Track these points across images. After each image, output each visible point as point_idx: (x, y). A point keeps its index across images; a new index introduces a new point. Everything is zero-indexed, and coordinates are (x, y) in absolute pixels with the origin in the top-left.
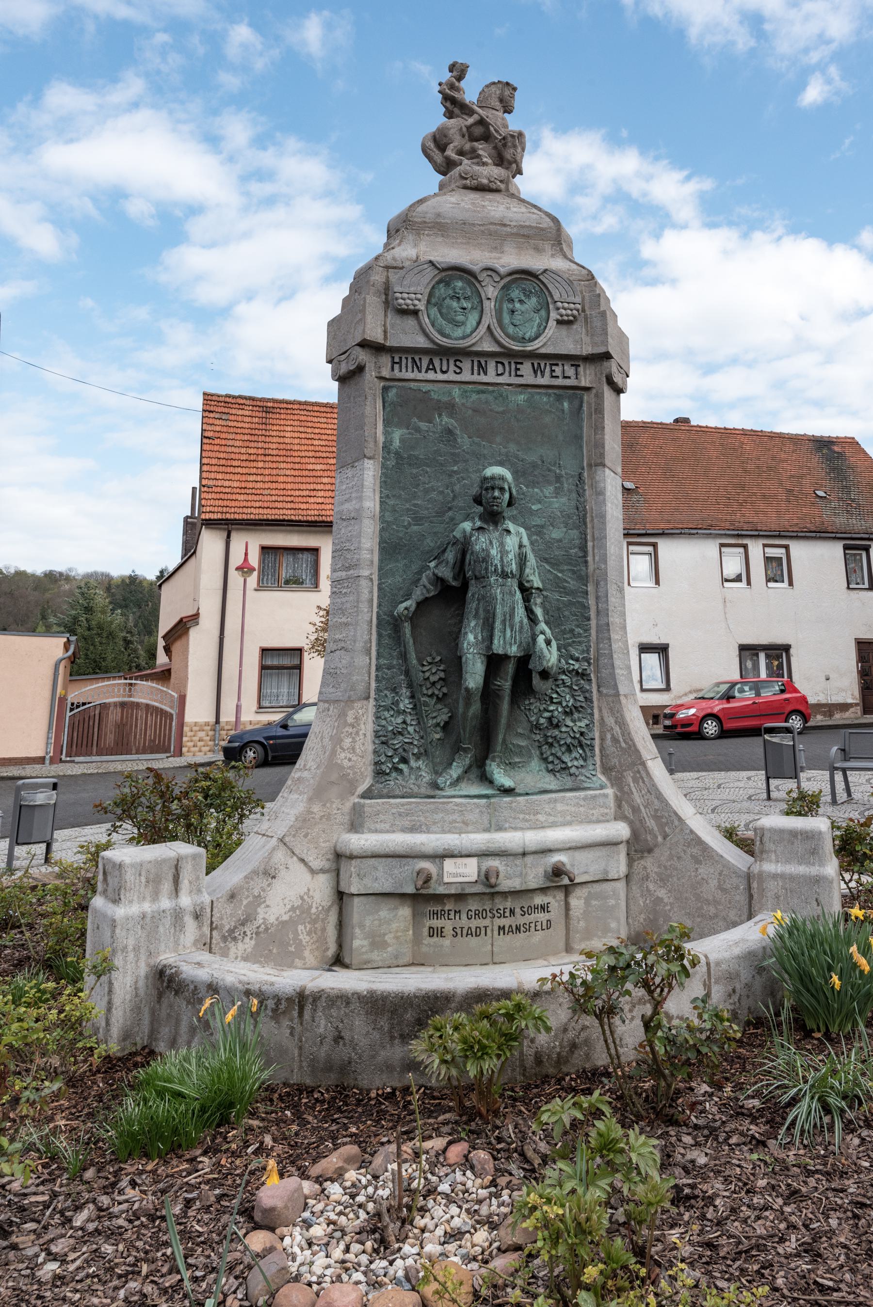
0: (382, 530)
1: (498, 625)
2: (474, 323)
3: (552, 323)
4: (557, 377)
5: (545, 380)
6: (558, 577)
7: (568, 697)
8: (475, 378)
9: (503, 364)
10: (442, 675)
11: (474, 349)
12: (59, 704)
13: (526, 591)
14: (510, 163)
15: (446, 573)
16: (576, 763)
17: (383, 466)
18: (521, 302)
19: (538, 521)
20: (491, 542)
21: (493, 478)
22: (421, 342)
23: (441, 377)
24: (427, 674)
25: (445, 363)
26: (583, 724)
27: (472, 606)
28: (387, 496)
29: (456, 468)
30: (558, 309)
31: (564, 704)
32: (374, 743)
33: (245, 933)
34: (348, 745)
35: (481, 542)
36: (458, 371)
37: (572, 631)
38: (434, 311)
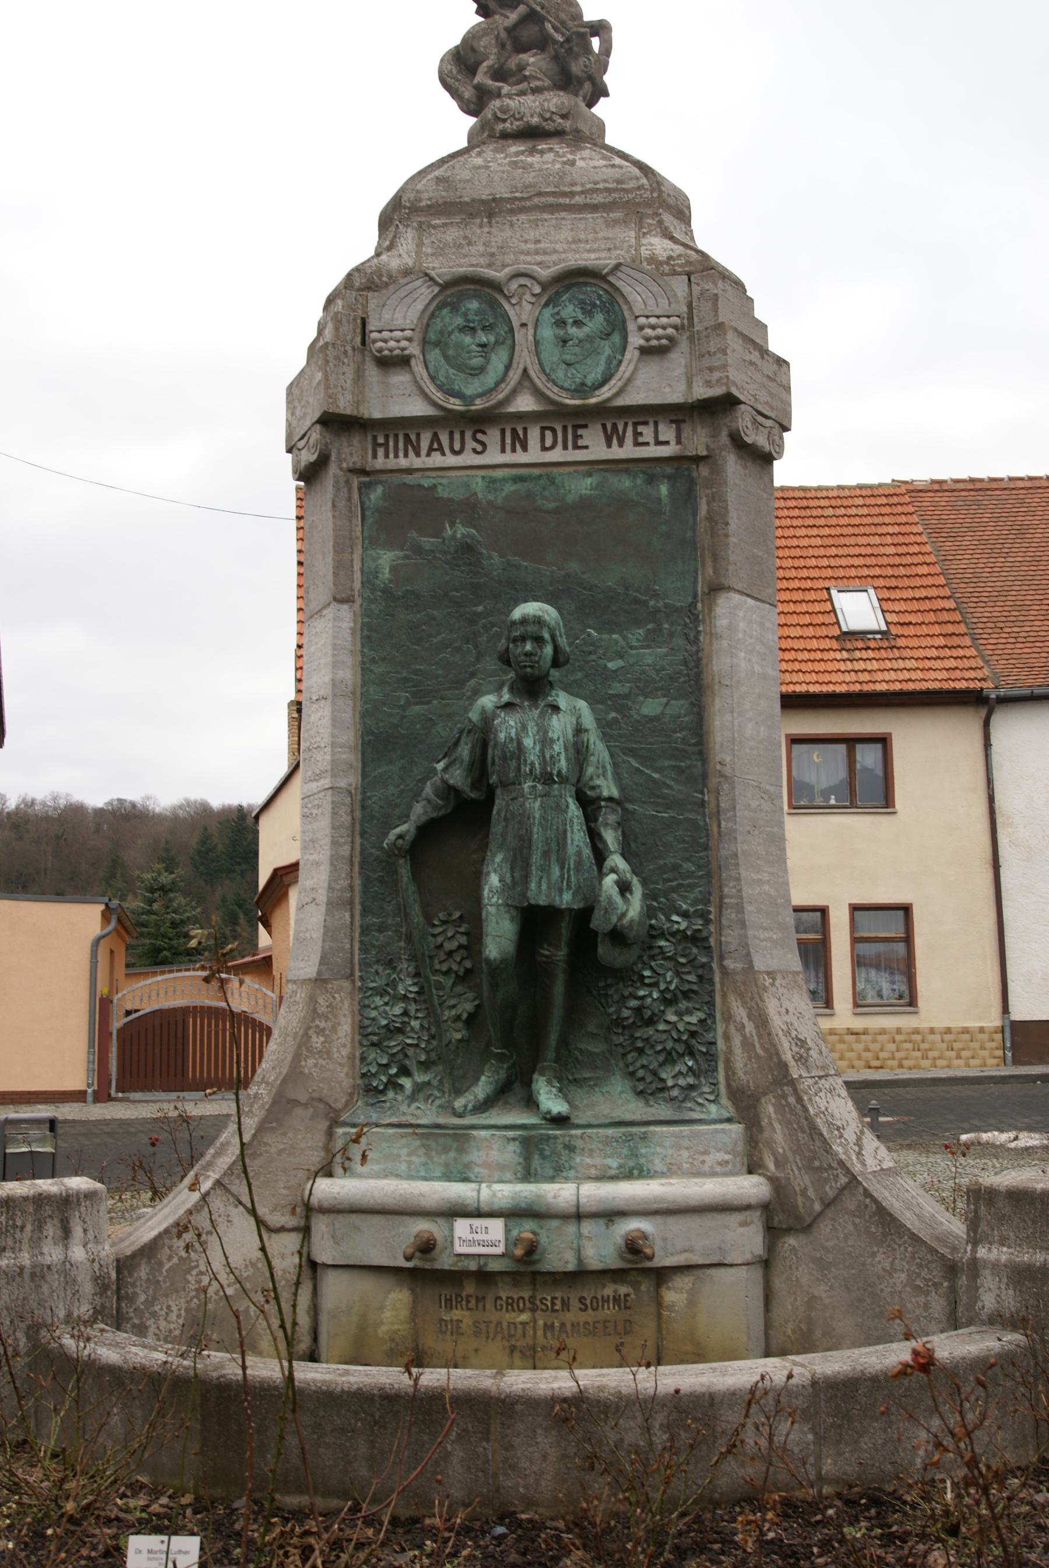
0: (364, 715)
1: (536, 858)
2: (501, 368)
3: (631, 354)
4: (647, 444)
5: (628, 451)
6: (654, 780)
7: (669, 975)
8: (508, 458)
9: (554, 431)
10: (463, 940)
12: (102, 1008)
13: (589, 804)
14: (580, 83)
15: (457, 777)
16: (682, 1082)
18: (577, 323)
19: (617, 688)
20: (524, 727)
21: (524, 621)
22: (417, 408)
23: (451, 460)
24: (440, 939)
25: (457, 437)
26: (694, 1019)
27: (497, 828)
28: (373, 661)
29: (480, 609)
30: (641, 328)
31: (662, 986)
32: (361, 1045)
33: (169, 1307)
35: (507, 726)
36: (479, 448)
37: (676, 867)
38: (434, 355)
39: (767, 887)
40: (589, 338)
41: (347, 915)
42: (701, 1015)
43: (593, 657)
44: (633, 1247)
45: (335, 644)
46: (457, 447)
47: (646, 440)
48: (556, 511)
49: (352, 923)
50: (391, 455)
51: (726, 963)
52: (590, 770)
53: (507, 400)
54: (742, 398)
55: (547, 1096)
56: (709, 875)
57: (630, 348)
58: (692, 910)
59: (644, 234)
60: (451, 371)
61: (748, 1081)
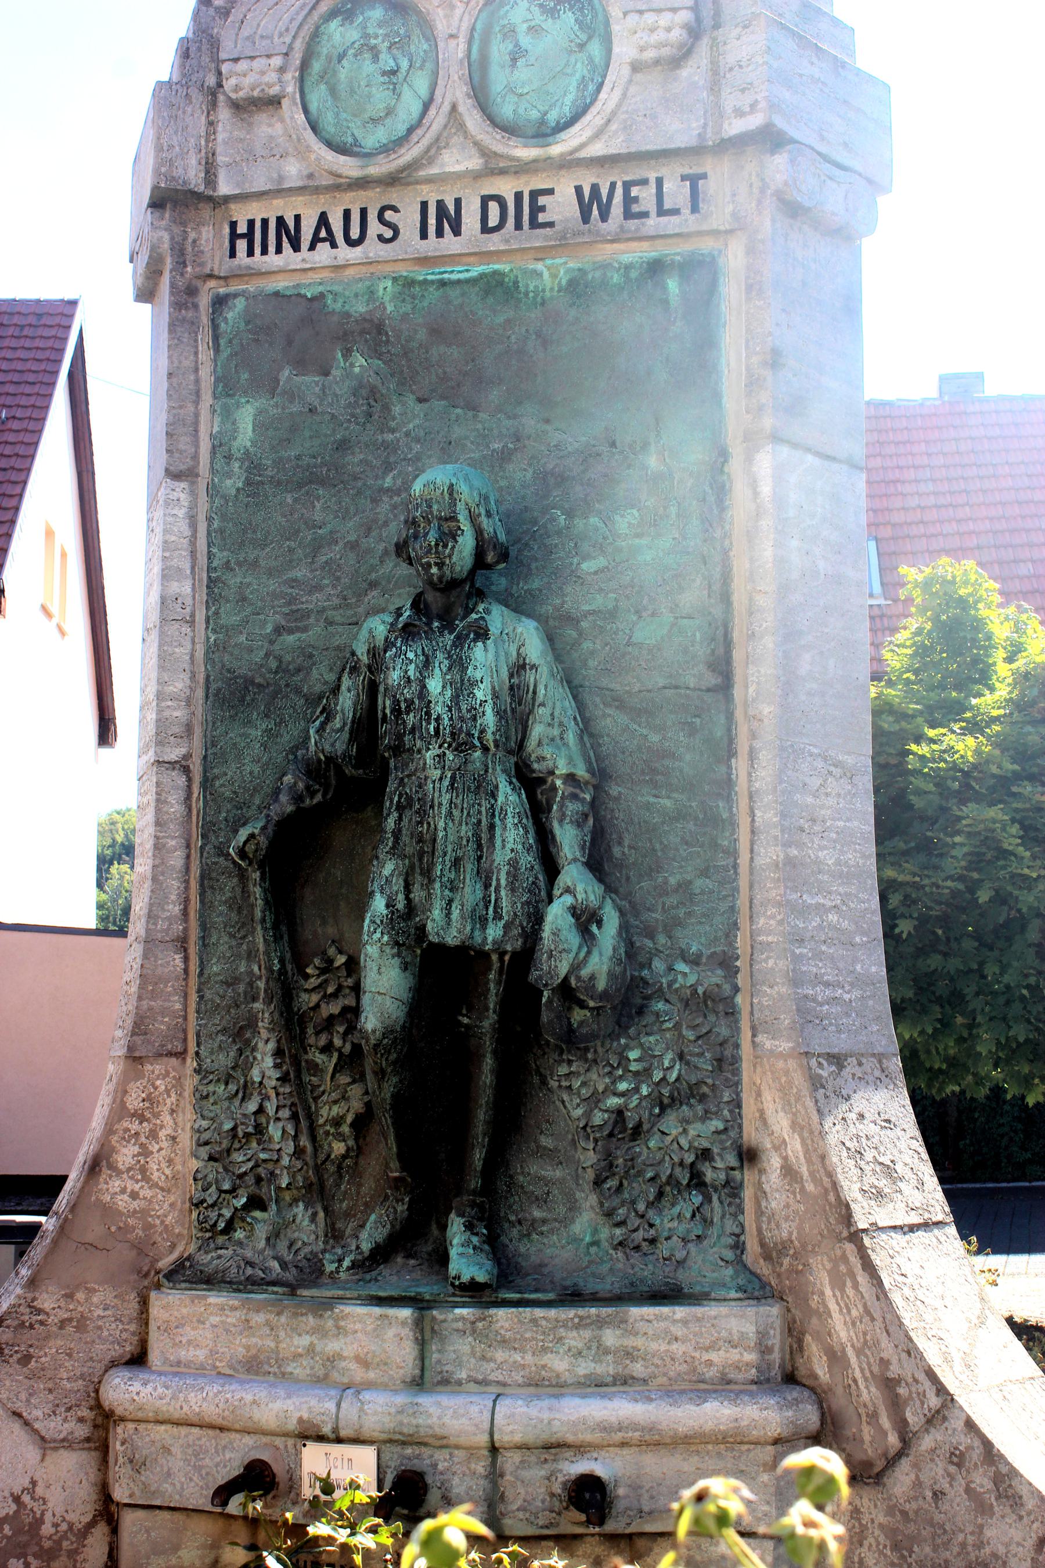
4: (675, 212)
11: (583, 154)
17: (212, 491)
29: (388, 482)
34: (129, 1161)
36: (388, 234)
39: (833, 917)
41: (178, 959)
45: (165, 542)
46: (355, 233)
47: (643, 209)
49: (186, 971)
50: (258, 250)
51: (759, 1039)
53: (429, 156)
54: (793, 133)
55: (461, 1250)
58: (707, 952)
61: (791, 1233)
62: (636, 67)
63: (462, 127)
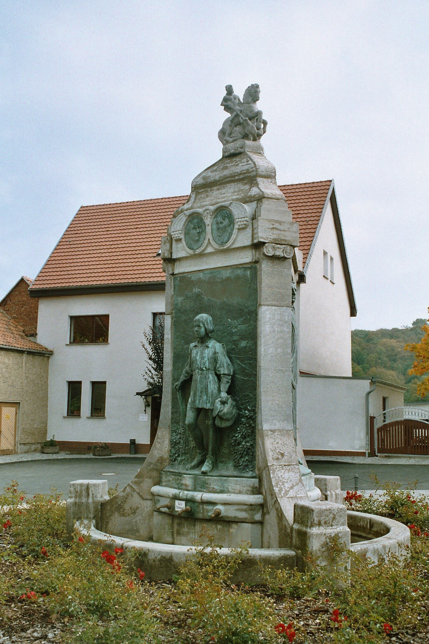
3: (235, 231)
18: (221, 223)
37: (248, 395)
40: (225, 227)
42: (251, 443)
43: (229, 328)
44: (218, 514)
48: (220, 282)
52: (218, 366)
56: (256, 398)
57: (235, 229)
59: (252, 187)
60: (191, 242)
62: (239, 229)
63: (210, 244)
